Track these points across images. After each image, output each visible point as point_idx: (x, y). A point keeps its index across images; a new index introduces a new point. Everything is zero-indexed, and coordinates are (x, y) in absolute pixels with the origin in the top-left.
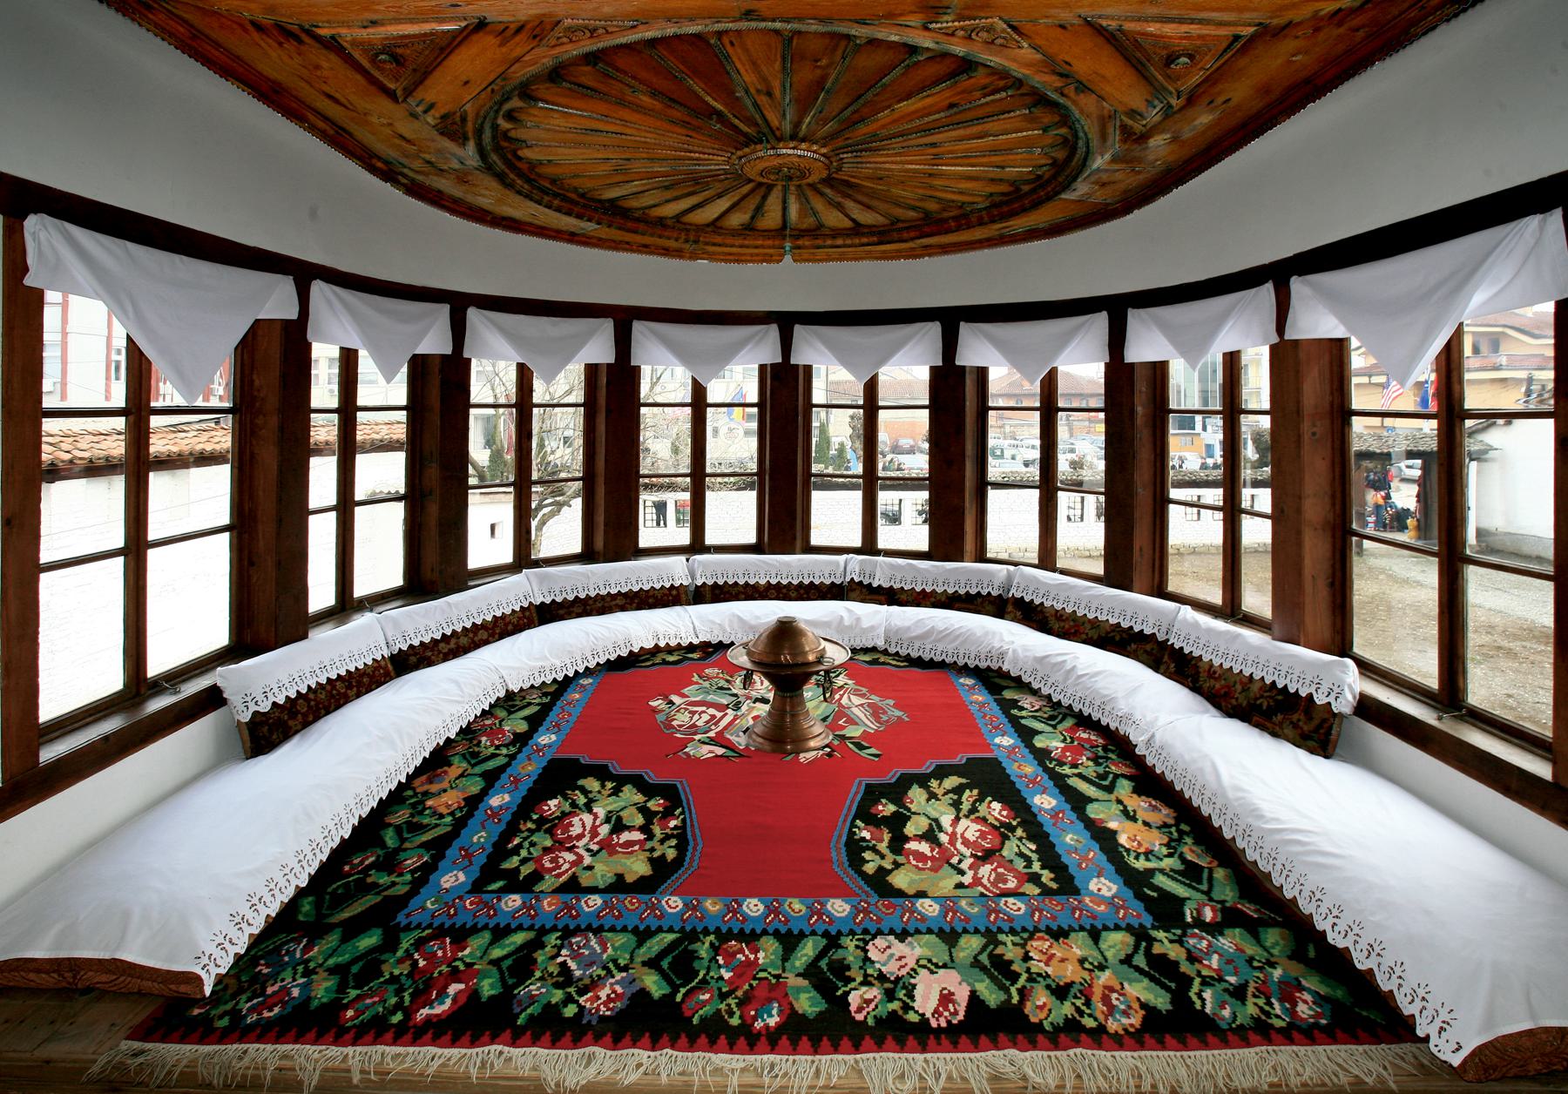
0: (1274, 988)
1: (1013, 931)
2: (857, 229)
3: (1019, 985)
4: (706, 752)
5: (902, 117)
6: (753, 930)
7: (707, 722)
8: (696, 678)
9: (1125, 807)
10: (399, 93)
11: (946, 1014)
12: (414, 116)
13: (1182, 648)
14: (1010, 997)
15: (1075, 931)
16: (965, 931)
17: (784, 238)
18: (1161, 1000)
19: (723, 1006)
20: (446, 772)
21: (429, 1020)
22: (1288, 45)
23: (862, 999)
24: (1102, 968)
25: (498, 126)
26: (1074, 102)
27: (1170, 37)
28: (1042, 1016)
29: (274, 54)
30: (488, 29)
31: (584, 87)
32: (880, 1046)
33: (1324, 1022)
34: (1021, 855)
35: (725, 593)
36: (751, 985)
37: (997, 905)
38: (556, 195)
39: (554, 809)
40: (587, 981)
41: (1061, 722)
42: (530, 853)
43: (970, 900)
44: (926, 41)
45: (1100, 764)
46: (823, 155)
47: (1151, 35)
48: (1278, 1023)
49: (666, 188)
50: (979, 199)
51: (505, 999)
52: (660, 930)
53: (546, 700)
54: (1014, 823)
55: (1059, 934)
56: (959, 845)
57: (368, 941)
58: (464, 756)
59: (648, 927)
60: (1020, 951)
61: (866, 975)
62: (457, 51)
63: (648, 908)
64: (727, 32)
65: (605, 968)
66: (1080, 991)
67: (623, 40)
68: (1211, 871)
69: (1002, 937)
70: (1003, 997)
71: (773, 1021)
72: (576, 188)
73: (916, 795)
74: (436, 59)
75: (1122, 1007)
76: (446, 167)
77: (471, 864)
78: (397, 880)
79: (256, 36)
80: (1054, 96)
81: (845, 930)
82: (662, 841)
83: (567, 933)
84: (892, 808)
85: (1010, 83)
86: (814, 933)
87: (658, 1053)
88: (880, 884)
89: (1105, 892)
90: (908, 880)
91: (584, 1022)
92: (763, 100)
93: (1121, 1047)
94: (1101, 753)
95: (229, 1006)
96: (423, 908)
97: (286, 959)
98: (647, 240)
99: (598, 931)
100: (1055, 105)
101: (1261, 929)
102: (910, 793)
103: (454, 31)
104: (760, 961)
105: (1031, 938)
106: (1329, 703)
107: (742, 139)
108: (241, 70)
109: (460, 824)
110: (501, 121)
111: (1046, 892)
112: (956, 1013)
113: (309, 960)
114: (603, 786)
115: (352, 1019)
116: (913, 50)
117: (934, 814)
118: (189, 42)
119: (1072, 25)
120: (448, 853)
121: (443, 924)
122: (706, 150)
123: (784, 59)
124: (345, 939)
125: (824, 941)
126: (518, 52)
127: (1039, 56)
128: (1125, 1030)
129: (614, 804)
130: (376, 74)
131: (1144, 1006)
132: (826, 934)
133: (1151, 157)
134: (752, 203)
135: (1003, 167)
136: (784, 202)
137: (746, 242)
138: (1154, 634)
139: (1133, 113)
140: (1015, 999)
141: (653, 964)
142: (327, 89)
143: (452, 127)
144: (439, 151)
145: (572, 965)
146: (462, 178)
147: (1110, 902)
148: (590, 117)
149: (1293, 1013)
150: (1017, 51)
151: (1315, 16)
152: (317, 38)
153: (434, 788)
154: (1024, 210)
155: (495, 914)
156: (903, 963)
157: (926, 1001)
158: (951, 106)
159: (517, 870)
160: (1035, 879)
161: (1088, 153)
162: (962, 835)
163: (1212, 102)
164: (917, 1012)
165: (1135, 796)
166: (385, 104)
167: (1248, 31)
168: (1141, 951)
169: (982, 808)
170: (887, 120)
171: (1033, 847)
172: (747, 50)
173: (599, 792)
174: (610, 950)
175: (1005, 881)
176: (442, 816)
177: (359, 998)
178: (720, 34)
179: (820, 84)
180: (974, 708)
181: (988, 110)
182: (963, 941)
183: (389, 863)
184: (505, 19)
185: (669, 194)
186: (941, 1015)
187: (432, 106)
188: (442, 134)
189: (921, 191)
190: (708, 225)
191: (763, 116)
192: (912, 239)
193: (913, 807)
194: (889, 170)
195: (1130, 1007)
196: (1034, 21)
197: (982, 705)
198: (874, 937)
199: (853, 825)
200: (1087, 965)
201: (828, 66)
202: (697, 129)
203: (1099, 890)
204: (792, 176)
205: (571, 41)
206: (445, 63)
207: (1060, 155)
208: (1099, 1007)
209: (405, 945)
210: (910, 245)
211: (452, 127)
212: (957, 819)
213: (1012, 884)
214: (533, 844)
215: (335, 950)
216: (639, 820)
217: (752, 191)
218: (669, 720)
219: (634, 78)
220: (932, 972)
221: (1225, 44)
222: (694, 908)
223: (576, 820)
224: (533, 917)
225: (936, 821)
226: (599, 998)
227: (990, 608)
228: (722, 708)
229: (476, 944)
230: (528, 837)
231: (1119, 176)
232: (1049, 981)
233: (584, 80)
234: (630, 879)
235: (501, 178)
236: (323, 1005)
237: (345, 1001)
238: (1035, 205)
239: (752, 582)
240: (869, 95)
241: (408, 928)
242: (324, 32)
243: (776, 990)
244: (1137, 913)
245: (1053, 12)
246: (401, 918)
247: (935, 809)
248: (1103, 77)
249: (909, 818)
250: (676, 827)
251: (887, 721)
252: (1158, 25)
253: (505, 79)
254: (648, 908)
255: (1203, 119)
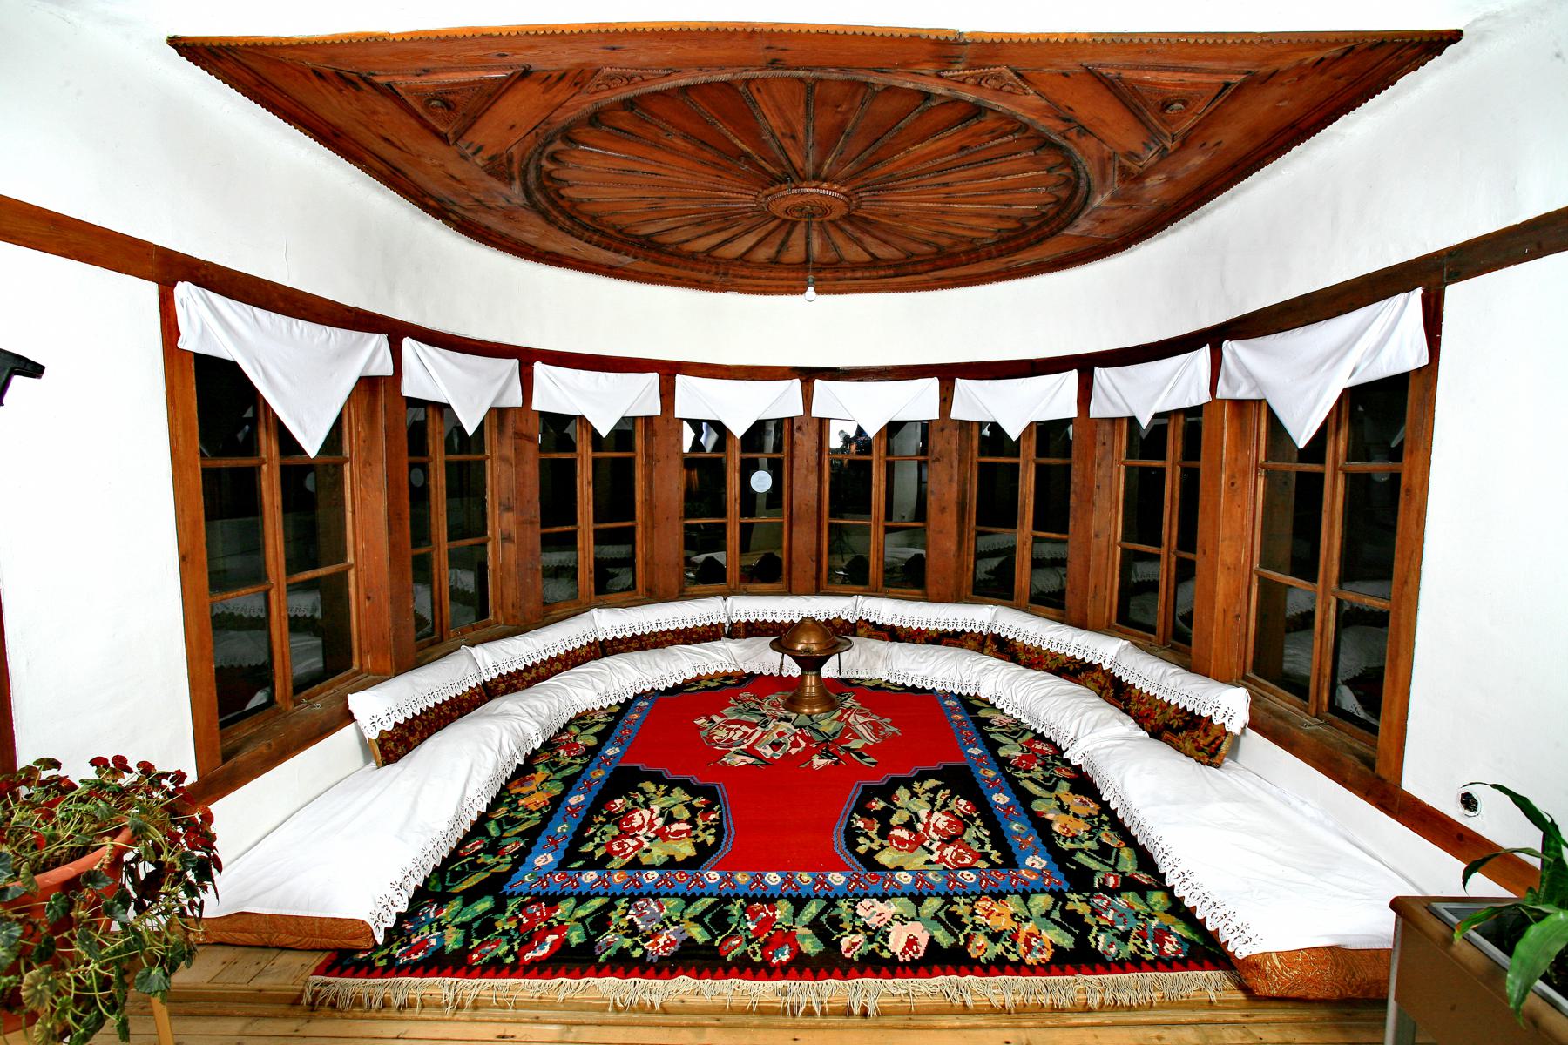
0: (1150, 934)
1: (965, 895)
2: (875, 263)
3: (965, 932)
4: (739, 761)
5: (917, 159)
6: (772, 895)
7: (741, 737)
8: (732, 701)
9: (1062, 802)
10: (450, 136)
11: (911, 952)
12: (464, 157)
13: (1120, 677)
14: (958, 940)
15: (1011, 894)
16: (930, 895)
17: (807, 270)
18: (1067, 942)
19: (749, 949)
20: (533, 778)
21: (533, 961)
22: (1275, 91)
23: (851, 943)
24: (1027, 920)
25: (542, 167)
26: (1076, 145)
27: (1166, 85)
28: (980, 953)
29: (334, 101)
30: (533, 76)
31: (621, 130)
32: (862, 974)
33: (1181, 955)
34: (977, 839)
35: (756, 630)
36: (770, 934)
37: (955, 876)
38: (596, 231)
39: (619, 806)
40: (649, 932)
41: (1021, 736)
42: (602, 840)
43: (936, 873)
44: (939, 89)
45: (1048, 770)
46: (843, 194)
47: (1148, 82)
48: (1148, 957)
49: (698, 224)
50: (989, 235)
51: (588, 947)
52: (702, 895)
53: (610, 720)
54: (975, 815)
55: (999, 896)
56: (931, 832)
57: (484, 905)
58: (546, 765)
59: (694, 894)
60: (969, 909)
61: (854, 926)
62: (503, 98)
63: (693, 879)
64: (754, 79)
65: (662, 923)
66: (1009, 936)
67: (658, 87)
68: (1119, 850)
69: (956, 899)
70: (953, 940)
71: (785, 958)
72: (614, 224)
73: (902, 794)
74: (484, 104)
75: (1038, 947)
76: (493, 205)
77: (557, 848)
78: (501, 860)
79: (317, 82)
80: (1057, 139)
81: (841, 895)
82: (704, 831)
83: (633, 899)
84: (882, 804)
85: (1017, 126)
86: (817, 897)
87: (701, 981)
88: (869, 860)
89: (1037, 866)
90: (890, 857)
91: (648, 960)
92: (787, 142)
93: (1034, 974)
94: (1050, 761)
95: (386, 952)
96: (523, 881)
97: (423, 918)
98: (681, 273)
99: (656, 897)
100: (1059, 147)
101: (1148, 892)
102: (898, 793)
103: (500, 78)
104: (777, 917)
105: (978, 899)
106: (1224, 724)
107: (768, 179)
108: (304, 115)
109: (546, 819)
110: (544, 163)
111: (993, 865)
112: (918, 952)
113: (440, 920)
114: (658, 788)
115: (477, 960)
116: (927, 96)
117: (914, 809)
118: (255, 88)
119: (1075, 73)
120: (539, 840)
121: (538, 893)
122: (735, 190)
123: (807, 105)
124: (466, 904)
125: (825, 903)
126: (561, 98)
127: (1044, 102)
128: (1039, 962)
129: (666, 802)
130: (429, 118)
131: (1054, 946)
132: (826, 898)
133: (1147, 196)
134: (777, 239)
135: (1010, 205)
136: (808, 237)
137: (772, 275)
138: (1100, 664)
139: (1131, 155)
140: (962, 942)
141: (697, 919)
142: (382, 132)
143: (499, 168)
144: (488, 190)
145: (638, 921)
146: (508, 215)
147: (1040, 873)
148: (627, 159)
149: (1161, 950)
150: (1024, 97)
151: (1300, 65)
152: (373, 85)
153: (524, 790)
154: (1030, 245)
155: (578, 885)
156: (881, 917)
157: (897, 943)
158: (962, 148)
159: (592, 853)
160: (986, 857)
161: (1089, 192)
162: (934, 825)
163: (1204, 144)
164: (889, 951)
165: (1071, 794)
166: (438, 146)
167: (1237, 79)
168: (1058, 909)
169: (952, 805)
170: (903, 161)
171: (987, 833)
172: (773, 97)
173: (655, 793)
174: (665, 911)
175: (963, 859)
176: (532, 812)
177: (480, 946)
178: (748, 81)
179: (840, 129)
180: (954, 725)
181: (996, 152)
182: (927, 902)
183: (494, 848)
184: (549, 67)
185: (701, 230)
186: (906, 953)
187: (480, 149)
188: (490, 174)
189: (934, 228)
190: (737, 259)
191: (788, 158)
192: (926, 272)
193: (899, 804)
194: (904, 208)
195: (1044, 947)
196: (1039, 70)
197: (960, 722)
198: (862, 899)
199: (851, 817)
200: (1017, 918)
201: (848, 112)
202: (727, 170)
203: (1033, 864)
204: (815, 214)
205: (610, 88)
206: (493, 109)
207: (1063, 194)
208: (1021, 946)
209: (511, 908)
210: (924, 277)
211: (499, 168)
212: (932, 812)
213: (967, 861)
214: (604, 833)
215: (459, 913)
216: (686, 815)
217: (778, 227)
218: (711, 735)
219: (668, 122)
220: (903, 924)
221: (1216, 92)
222: (729, 880)
223: (637, 815)
224: (606, 887)
225: (916, 814)
226: (658, 944)
227: (971, 643)
228: (753, 725)
229: (563, 909)
230: (600, 828)
231: (1117, 213)
232: (988, 930)
233: (622, 124)
234: (679, 858)
235: (544, 215)
236: (454, 950)
237: (471, 947)
238: (1040, 240)
239: (778, 620)
240: (886, 138)
241: (512, 896)
242: (381, 80)
243: (789, 937)
244: (1058, 880)
245: (1057, 61)
246: (506, 888)
247: (915, 805)
248: (1103, 121)
249: (895, 812)
250: (715, 820)
251: (884, 736)
252: (1154, 73)
253: (548, 123)
254: (693, 879)
255: (1196, 160)
